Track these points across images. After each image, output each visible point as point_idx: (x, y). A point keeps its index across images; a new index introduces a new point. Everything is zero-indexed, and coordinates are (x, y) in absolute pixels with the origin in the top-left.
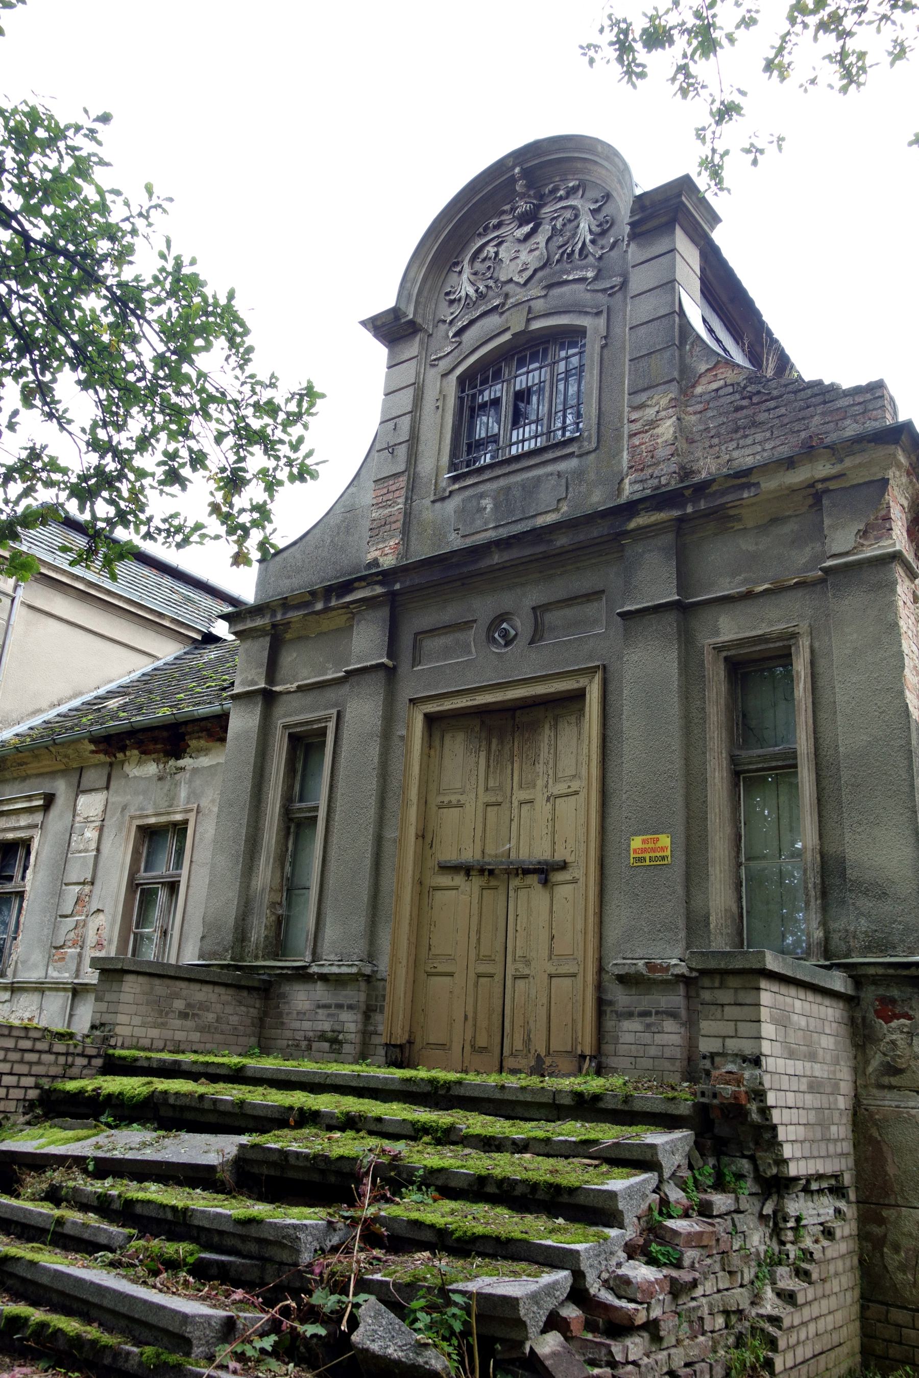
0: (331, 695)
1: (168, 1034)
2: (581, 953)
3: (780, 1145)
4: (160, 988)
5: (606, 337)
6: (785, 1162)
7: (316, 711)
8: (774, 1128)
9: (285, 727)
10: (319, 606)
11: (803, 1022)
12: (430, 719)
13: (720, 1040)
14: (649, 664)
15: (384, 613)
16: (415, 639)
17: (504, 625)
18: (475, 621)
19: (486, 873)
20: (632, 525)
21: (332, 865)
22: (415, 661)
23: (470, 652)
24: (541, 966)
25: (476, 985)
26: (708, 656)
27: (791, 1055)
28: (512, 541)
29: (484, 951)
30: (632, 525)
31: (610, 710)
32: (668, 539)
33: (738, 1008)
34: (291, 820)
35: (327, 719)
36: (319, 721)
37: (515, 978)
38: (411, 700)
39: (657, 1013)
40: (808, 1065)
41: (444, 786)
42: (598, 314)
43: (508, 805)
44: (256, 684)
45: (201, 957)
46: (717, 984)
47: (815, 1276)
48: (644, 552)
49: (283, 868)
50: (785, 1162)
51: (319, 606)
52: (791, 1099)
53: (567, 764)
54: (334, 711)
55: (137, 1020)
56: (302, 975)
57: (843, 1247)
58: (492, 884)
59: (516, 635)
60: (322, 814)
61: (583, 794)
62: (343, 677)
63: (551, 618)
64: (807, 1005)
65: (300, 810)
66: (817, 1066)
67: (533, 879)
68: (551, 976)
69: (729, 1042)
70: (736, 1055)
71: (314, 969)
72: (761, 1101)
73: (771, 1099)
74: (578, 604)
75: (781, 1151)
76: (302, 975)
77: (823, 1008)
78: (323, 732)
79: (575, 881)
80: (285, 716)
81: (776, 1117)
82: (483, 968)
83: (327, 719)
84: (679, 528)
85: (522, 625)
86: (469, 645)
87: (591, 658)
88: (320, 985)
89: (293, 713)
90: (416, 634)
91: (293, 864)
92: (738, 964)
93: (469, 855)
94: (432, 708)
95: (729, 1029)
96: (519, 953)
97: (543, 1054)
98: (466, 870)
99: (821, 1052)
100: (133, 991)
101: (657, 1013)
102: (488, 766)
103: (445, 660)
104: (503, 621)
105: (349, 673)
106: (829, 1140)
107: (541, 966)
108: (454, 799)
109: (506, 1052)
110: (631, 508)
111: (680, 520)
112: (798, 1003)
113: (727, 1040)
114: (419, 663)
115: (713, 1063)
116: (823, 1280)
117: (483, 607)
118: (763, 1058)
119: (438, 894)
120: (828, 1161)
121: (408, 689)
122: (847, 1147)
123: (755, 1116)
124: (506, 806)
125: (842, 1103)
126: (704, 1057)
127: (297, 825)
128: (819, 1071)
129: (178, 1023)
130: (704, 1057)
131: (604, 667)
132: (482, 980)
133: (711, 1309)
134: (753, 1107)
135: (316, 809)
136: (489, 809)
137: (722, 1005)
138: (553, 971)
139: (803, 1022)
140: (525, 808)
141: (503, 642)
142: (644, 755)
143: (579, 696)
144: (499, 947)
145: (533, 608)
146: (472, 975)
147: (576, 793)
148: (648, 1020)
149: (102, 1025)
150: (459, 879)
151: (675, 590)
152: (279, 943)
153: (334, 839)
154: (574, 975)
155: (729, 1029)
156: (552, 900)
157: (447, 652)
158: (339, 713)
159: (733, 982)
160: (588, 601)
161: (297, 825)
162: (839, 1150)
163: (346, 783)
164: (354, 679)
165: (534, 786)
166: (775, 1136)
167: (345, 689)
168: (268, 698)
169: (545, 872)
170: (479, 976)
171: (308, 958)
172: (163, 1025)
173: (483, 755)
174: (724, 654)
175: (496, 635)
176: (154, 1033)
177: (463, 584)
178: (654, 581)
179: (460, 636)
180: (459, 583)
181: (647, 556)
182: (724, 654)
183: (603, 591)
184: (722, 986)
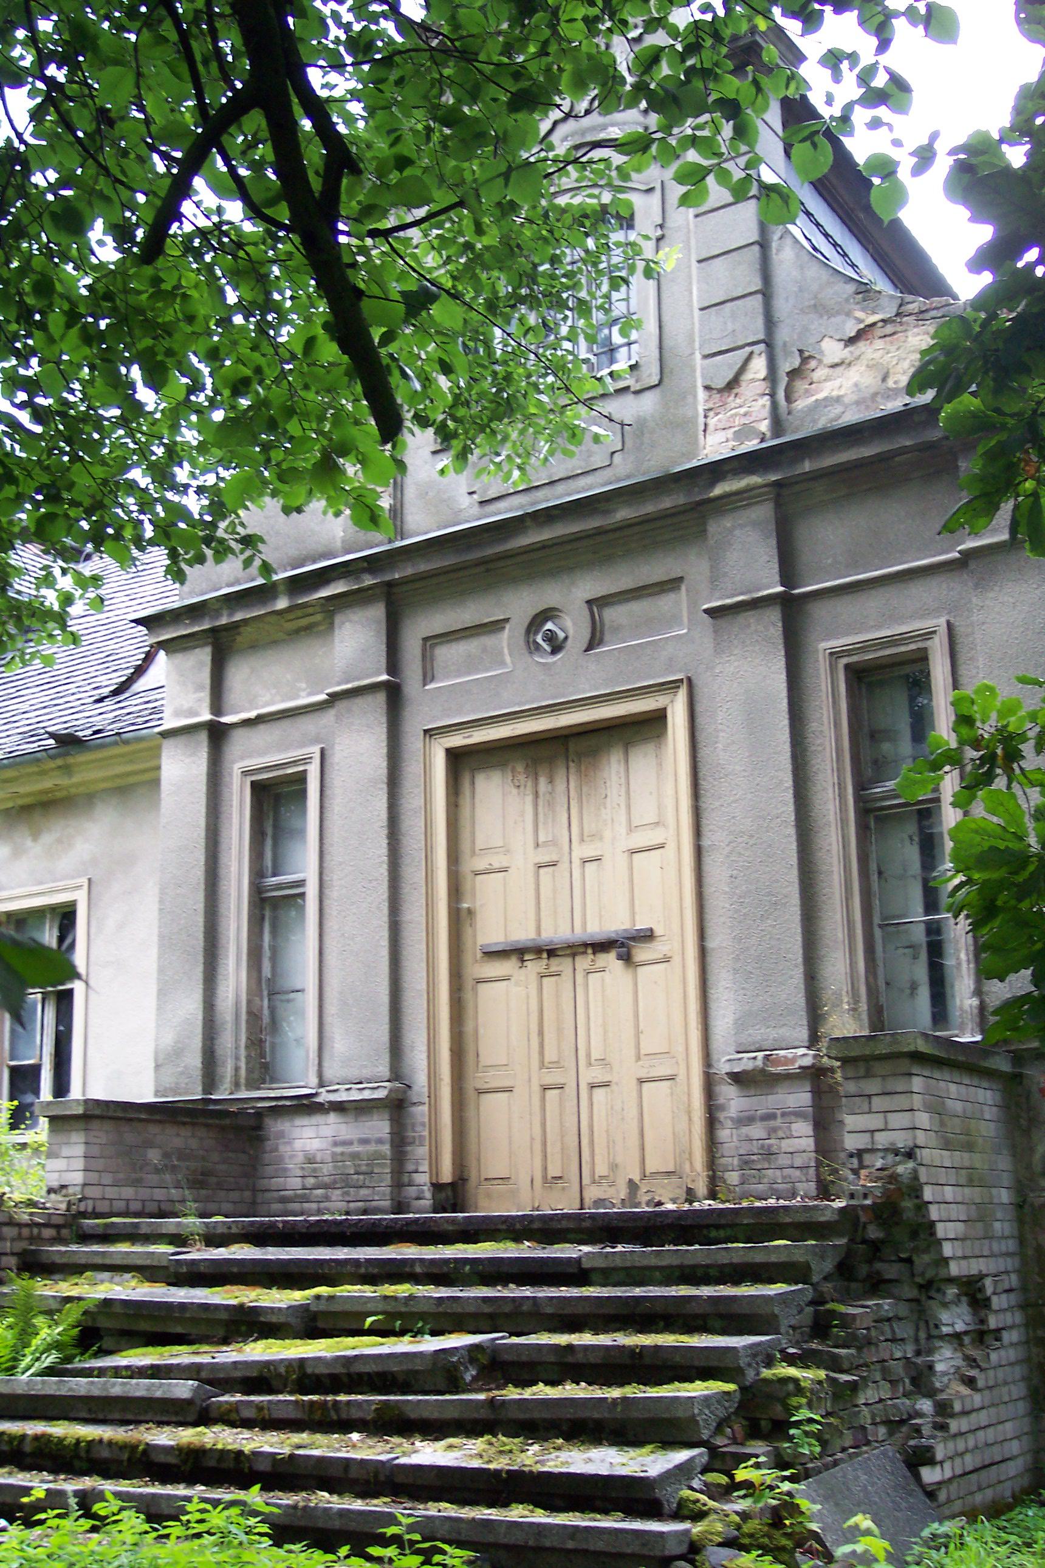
0: (308, 725)
1: (144, 1193)
2: (681, 1049)
3: (939, 1242)
4: (896, 1049)
5: (661, 226)
6: (946, 1261)
7: (287, 749)
8: (932, 1224)
9: (245, 773)
10: (282, 604)
11: (958, 1107)
12: (455, 757)
13: (868, 1135)
14: (747, 676)
15: (377, 612)
16: (424, 645)
17: (549, 626)
18: (507, 620)
19: (545, 955)
20: (718, 490)
21: (331, 959)
22: (428, 676)
23: (503, 664)
24: (626, 1072)
25: (543, 1099)
26: (822, 665)
27: (947, 1146)
28: (556, 512)
29: (550, 1055)
30: (718, 490)
31: (701, 737)
32: (764, 512)
33: (887, 1098)
34: (263, 900)
35: (306, 760)
36: (294, 763)
37: (592, 1087)
38: (426, 731)
39: (783, 1115)
40: (966, 1155)
41: (480, 844)
42: (650, 190)
43: (567, 865)
44: (197, 714)
45: (157, 1093)
46: (862, 1072)
47: (981, 1383)
48: (734, 528)
49: (259, 970)
50: (946, 1261)
51: (282, 604)
52: (949, 1193)
53: (646, 811)
54: (316, 750)
55: (107, 1179)
56: (306, 1106)
57: (1012, 1354)
58: (553, 969)
59: (566, 638)
60: (311, 890)
61: (671, 847)
62: (325, 702)
63: (612, 615)
64: (963, 1089)
65: (280, 887)
66: (977, 1156)
67: (610, 959)
68: (641, 1081)
69: (878, 1136)
70: (886, 1150)
71: (324, 1097)
72: (917, 1197)
73: (928, 1194)
74: (650, 595)
75: (940, 1251)
76: (306, 1106)
77: (981, 1091)
78: (301, 778)
79: (666, 960)
80: (242, 758)
81: (934, 1213)
82: (549, 1080)
83: (306, 760)
84: (778, 495)
85: (573, 625)
86: (501, 653)
87: (669, 670)
88: (332, 1117)
89: (253, 756)
90: (425, 639)
91: (274, 959)
92: (883, 1049)
93: (523, 933)
94: (457, 740)
95: (874, 1121)
96: (595, 1055)
97: (636, 1178)
98: (519, 952)
99: (980, 1140)
100: (98, 1141)
101: (783, 1115)
102: (536, 814)
103: (469, 674)
104: (546, 620)
105: (334, 697)
106: (992, 1238)
107: (626, 1072)
108: (497, 862)
109: (586, 1180)
110: (717, 470)
111: (777, 484)
112: (953, 1087)
113: (877, 1134)
114: (433, 679)
115: (861, 1161)
116: (990, 1388)
117: (519, 604)
118: (918, 1150)
119: (482, 987)
120: (991, 1260)
121: (421, 714)
122: (1011, 1245)
123: (909, 1215)
124: (564, 866)
125: (1005, 1196)
126: (851, 1156)
127: (273, 906)
128: (977, 1160)
129: (153, 1179)
130: (851, 1156)
131: (689, 679)
132: (549, 1093)
133: (873, 1418)
134: (907, 1204)
135: (301, 883)
136: (542, 871)
137: (869, 1096)
138: (643, 1074)
139: (958, 1107)
140: (590, 867)
141: (548, 649)
142: (749, 796)
143: (656, 721)
144: (569, 1052)
145: (589, 602)
146: (536, 1088)
147: (661, 846)
148: (772, 1123)
149: (63, 1187)
150: (507, 967)
151: (777, 578)
152: (263, 1065)
153: (331, 924)
154: (671, 1078)
155: (874, 1121)
156: (636, 984)
157: (471, 665)
158: (322, 751)
159: (879, 1068)
160: (663, 591)
161: (273, 906)
162: (1004, 1249)
163: (339, 849)
164: (342, 705)
165: (601, 839)
166: (933, 1234)
167: (328, 718)
168: (217, 735)
169: (623, 947)
170: (545, 1089)
171: (314, 1080)
172: (136, 1183)
173: (529, 799)
174: (845, 661)
175: (539, 639)
176: (128, 1192)
177: (487, 571)
178: (745, 559)
179: (488, 641)
180: (482, 568)
181: (737, 532)
182: (845, 661)
183: (681, 579)
184: (868, 1075)
